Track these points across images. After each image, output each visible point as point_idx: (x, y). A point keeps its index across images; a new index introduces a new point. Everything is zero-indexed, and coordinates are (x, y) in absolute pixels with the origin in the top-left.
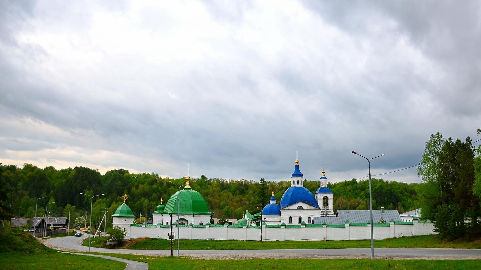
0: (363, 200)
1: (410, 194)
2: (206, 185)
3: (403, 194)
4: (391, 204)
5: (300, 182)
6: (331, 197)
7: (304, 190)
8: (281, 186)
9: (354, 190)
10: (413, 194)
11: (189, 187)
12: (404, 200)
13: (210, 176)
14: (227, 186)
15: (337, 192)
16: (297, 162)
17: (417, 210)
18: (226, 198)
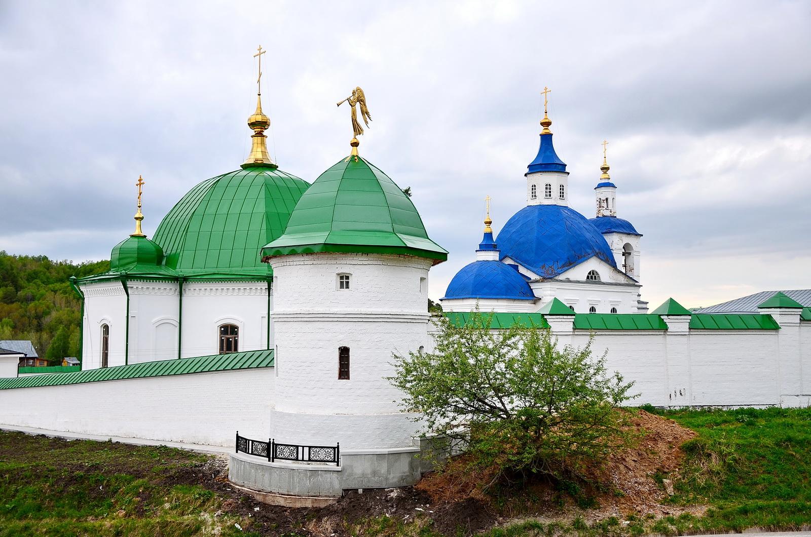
16: (547, 124)
17: (798, 302)
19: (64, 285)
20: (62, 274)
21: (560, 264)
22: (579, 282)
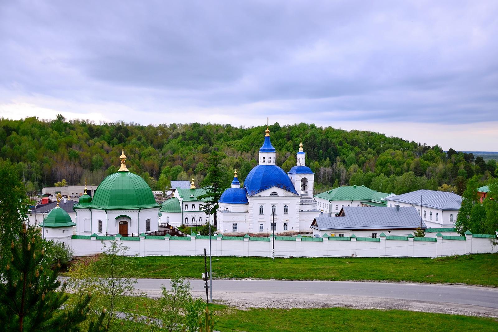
0: (291, 152)
1: (351, 145)
2: (66, 130)
3: (342, 146)
4: (328, 159)
5: (272, 159)
6: (310, 178)
7: (278, 170)
8: (175, 131)
9: (277, 139)
10: (355, 146)
11: (126, 170)
12: (344, 154)
13: (69, 117)
14: (99, 132)
15: (255, 140)
18: (99, 150)
19: (235, 142)
20: (235, 135)
21: (258, 190)
22: (266, 197)
